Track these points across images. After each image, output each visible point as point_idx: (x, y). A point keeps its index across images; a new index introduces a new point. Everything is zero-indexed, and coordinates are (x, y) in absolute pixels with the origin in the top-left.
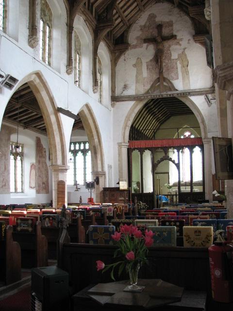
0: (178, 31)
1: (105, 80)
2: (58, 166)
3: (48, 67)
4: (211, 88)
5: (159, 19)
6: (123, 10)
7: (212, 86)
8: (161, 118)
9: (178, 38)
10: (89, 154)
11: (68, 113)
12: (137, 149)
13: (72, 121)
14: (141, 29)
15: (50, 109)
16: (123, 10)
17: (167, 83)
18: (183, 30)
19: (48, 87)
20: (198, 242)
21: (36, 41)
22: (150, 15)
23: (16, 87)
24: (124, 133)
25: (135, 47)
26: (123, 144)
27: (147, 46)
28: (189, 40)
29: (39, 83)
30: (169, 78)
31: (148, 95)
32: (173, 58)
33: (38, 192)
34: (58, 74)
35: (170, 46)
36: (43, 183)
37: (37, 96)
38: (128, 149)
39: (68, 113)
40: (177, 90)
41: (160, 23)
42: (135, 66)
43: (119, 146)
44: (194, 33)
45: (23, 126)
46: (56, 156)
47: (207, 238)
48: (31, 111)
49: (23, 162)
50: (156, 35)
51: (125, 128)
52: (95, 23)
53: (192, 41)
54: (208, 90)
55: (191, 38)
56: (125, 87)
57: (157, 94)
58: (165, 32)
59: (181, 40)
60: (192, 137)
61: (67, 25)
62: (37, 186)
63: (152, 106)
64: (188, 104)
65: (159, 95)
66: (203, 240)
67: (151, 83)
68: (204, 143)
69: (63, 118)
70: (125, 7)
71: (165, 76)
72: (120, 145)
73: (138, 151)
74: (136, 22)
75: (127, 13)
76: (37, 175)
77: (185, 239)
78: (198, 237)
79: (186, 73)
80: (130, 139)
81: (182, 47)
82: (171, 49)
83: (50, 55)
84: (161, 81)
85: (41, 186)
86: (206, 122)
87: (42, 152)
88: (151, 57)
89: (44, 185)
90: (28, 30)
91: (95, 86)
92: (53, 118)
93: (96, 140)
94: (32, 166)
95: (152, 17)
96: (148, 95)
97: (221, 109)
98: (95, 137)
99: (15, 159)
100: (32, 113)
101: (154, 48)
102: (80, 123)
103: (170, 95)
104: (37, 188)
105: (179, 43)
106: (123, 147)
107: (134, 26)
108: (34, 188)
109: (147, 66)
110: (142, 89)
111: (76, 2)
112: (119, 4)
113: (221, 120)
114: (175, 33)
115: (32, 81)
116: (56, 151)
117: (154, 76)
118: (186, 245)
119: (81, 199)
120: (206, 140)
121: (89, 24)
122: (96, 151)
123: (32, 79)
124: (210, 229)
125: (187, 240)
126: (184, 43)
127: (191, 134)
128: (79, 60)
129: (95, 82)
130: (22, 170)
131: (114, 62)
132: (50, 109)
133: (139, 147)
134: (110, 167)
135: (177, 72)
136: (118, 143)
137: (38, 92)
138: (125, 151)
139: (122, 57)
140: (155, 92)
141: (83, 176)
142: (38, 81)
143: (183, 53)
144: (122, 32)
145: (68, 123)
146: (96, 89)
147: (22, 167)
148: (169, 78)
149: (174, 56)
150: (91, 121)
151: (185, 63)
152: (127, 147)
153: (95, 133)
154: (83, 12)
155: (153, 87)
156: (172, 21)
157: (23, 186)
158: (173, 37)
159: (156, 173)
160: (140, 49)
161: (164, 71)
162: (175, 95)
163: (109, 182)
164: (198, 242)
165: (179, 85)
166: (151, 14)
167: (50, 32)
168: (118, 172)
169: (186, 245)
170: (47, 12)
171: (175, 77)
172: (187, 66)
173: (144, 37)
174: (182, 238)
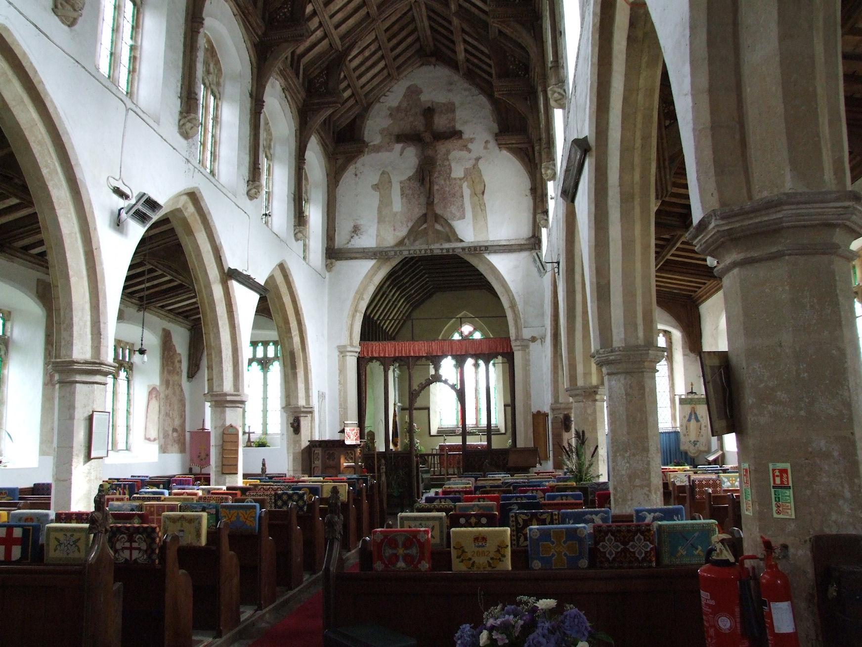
0: (465, 122)
1: (315, 215)
2: (226, 395)
3: (210, 177)
4: (529, 239)
5: (426, 97)
6: (358, 73)
7: (531, 235)
8: (427, 294)
9: (465, 136)
10: (276, 369)
11: (247, 281)
12: (377, 359)
13: (255, 297)
14: (391, 115)
15: (213, 273)
16: (358, 73)
17: (442, 225)
18: (475, 121)
19: (211, 224)
20: (481, 561)
21: (195, 125)
22: (409, 88)
23: (155, 217)
24: (352, 325)
25: (377, 149)
26: (349, 349)
27: (403, 150)
28: (487, 142)
29: (192, 214)
30: (447, 215)
31: (403, 248)
32: (453, 175)
33: (163, 450)
34: (233, 198)
35: (448, 152)
36: (175, 430)
37: (185, 240)
38: (359, 359)
39: (247, 281)
40: (462, 241)
41: (429, 105)
42: (376, 187)
43: (341, 352)
44: (497, 131)
45: (136, 304)
46: (221, 371)
47: (498, 551)
48: (160, 272)
49: (132, 383)
50: (422, 128)
51: (354, 316)
52: (302, 95)
53: (492, 144)
54: (523, 242)
55: (490, 138)
56: (356, 230)
57: (419, 247)
58: (441, 122)
59: (471, 140)
60: (477, 336)
61: (251, 95)
62: (161, 436)
63: (400, 272)
64: (482, 268)
65: (426, 250)
66: (492, 555)
67: (410, 225)
68: (514, 348)
69: (236, 287)
70: (363, 69)
71: (439, 211)
72: (342, 351)
73: (378, 363)
74: (381, 100)
75: (364, 80)
76: (163, 413)
77: (454, 553)
78: (480, 549)
79: (480, 208)
80: (361, 339)
81: (474, 155)
82: (450, 157)
83: (214, 155)
84: (428, 221)
85: (170, 437)
86: (520, 307)
87: (173, 363)
88: (410, 173)
89: (175, 434)
90: (179, 100)
91: (299, 225)
92: (218, 291)
93: (296, 339)
94: (152, 391)
95: (413, 92)
96: (403, 248)
97: (598, 283)
98: (295, 333)
99: (476, 365)
100: (162, 276)
101: (416, 155)
102: (272, 304)
103: (448, 250)
104: (162, 441)
105: (465, 146)
106: (348, 354)
107: (377, 106)
108: (155, 440)
109: (402, 188)
110: (391, 237)
111: (272, 52)
112: (351, 61)
113: (599, 308)
114: (458, 127)
115: (179, 210)
116: (221, 362)
117: (417, 210)
118: (458, 566)
119: (264, 465)
120: (518, 343)
121: (292, 97)
122: (292, 362)
123: (180, 206)
124: (505, 531)
125: (458, 557)
126: (477, 148)
127: (475, 329)
128: (269, 169)
129: (300, 219)
130: (129, 401)
131: (334, 177)
132: (213, 273)
133: (382, 355)
134: (322, 396)
135: (462, 206)
136: (338, 347)
137: (190, 232)
138: (352, 363)
139: (351, 169)
140: (417, 243)
141: (261, 414)
142: (191, 209)
143: (474, 166)
144: (352, 117)
145: (246, 301)
146: (300, 232)
147: (128, 394)
148: (445, 216)
149: (458, 172)
150: (287, 300)
151: (479, 188)
152: (357, 355)
153: (294, 325)
154: (281, 71)
155: (413, 233)
156: (453, 104)
157: (131, 437)
158: (456, 134)
159: (416, 409)
160: (388, 154)
161: (436, 201)
162: (457, 252)
163: (322, 427)
164: (481, 561)
165: (468, 232)
166: (411, 85)
167: (216, 108)
168: (338, 407)
169: (458, 566)
170: (212, 66)
171: (458, 214)
172: (483, 193)
173: (396, 131)
174: (450, 552)
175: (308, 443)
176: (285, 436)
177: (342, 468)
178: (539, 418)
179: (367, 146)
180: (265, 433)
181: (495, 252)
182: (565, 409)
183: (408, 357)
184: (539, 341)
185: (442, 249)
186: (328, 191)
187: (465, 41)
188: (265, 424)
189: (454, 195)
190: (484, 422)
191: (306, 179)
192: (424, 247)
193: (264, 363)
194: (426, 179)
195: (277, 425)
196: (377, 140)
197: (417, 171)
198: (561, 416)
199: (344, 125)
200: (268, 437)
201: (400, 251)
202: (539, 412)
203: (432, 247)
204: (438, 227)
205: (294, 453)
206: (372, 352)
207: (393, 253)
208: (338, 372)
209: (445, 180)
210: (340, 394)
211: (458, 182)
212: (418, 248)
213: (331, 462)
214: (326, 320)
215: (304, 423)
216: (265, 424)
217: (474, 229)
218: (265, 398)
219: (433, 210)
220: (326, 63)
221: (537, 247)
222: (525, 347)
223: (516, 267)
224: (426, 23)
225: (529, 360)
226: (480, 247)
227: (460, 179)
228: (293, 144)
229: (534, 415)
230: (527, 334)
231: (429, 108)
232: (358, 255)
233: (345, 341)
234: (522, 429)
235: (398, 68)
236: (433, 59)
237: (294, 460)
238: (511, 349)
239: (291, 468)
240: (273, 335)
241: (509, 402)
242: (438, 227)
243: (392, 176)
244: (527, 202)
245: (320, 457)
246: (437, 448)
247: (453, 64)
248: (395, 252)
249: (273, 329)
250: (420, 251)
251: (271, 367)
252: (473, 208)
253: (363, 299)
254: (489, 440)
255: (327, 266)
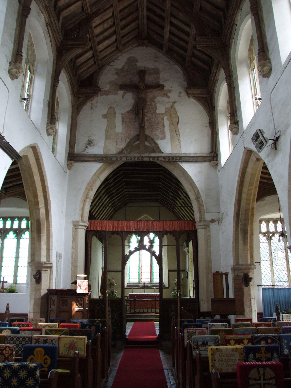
1: (62, 129)
7: (210, 151)
9: (166, 88)
10: (26, 236)
14: (117, 73)
17: (149, 142)
18: (173, 80)
24: (83, 207)
25: (107, 93)
26: (81, 223)
27: (124, 95)
28: (180, 93)
30: (153, 136)
31: (123, 155)
32: (158, 111)
35: (155, 97)
40: (163, 153)
43: (75, 226)
51: (85, 201)
53: (184, 94)
54: (206, 155)
56: (90, 143)
57: (134, 156)
58: (150, 79)
59: (170, 91)
63: (112, 185)
64: (176, 173)
65: (138, 157)
67: (128, 141)
71: (147, 133)
72: (76, 225)
74: (111, 64)
79: (176, 133)
81: (172, 100)
82: (156, 100)
86: (203, 198)
88: (129, 109)
93: (42, 211)
95: (132, 61)
98: (42, 205)
105: (166, 94)
106: (80, 227)
107: (108, 68)
109: (123, 118)
110: (113, 149)
114: (161, 83)
120: (202, 223)
126: (173, 96)
129: (52, 118)
131: (77, 108)
133: (104, 229)
134: (59, 256)
135: (164, 131)
138: (82, 233)
139: (89, 104)
141: (13, 269)
143: (171, 107)
144: (91, 73)
146: (51, 128)
148: (152, 137)
149: (161, 109)
150: (37, 178)
153: (41, 199)
154: (46, 6)
158: (159, 87)
161: (146, 127)
163: (56, 279)
165: (167, 147)
168: (70, 265)
171: (161, 136)
172: (178, 124)
175: (46, 291)
176: (29, 285)
177: (73, 313)
178: (218, 277)
179: (100, 91)
180: (15, 282)
181: (186, 161)
182: (245, 269)
183: (122, 232)
184: (217, 222)
185: (150, 157)
186: (72, 117)
187: (171, 24)
188: (16, 276)
189: (158, 124)
190: (156, 280)
191: (58, 105)
192: (137, 155)
193: (19, 233)
194: (140, 113)
195: (23, 277)
196: (107, 87)
197: (133, 108)
198: (242, 275)
199: (87, 76)
200: (17, 285)
201: (121, 157)
202: (217, 272)
203: (143, 155)
204: (147, 143)
205: (35, 299)
206: (97, 227)
207: (115, 159)
208: (72, 239)
209: (152, 115)
210: (72, 256)
211: (161, 115)
212: (133, 155)
213: (65, 308)
214: (65, 203)
215: (45, 276)
216: (16, 276)
217: (171, 146)
218: (17, 257)
219: (144, 132)
220: (78, 21)
221: (215, 159)
222: (207, 226)
223: (200, 172)
224: (145, 13)
225: (209, 236)
226: (176, 157)
227: (163, 114)
228: (50, 68)
229: (214, 274)
230: (208, 217)
231: (142, 70)
232: (90, 159)
233: (77, 217)
234: (205, 284)
235: (124, 45)
236: (146, 42)
237: (35, 304)
238: (195, 228)
239: (32, 311)
240: (25, 212)
241: (175, 267)
242: (147, 143)
243: (116, 110)
244: (207, 131)
245: (56, 303)
246: (128, 296)
247: (159, 46)
248: (117, 158)
249: (24, 207)
250: (134, 158)
251: (23, 235)
252: (171, 133)
253: (92, 190)
254: (161, 292)
255: (68, 165)
